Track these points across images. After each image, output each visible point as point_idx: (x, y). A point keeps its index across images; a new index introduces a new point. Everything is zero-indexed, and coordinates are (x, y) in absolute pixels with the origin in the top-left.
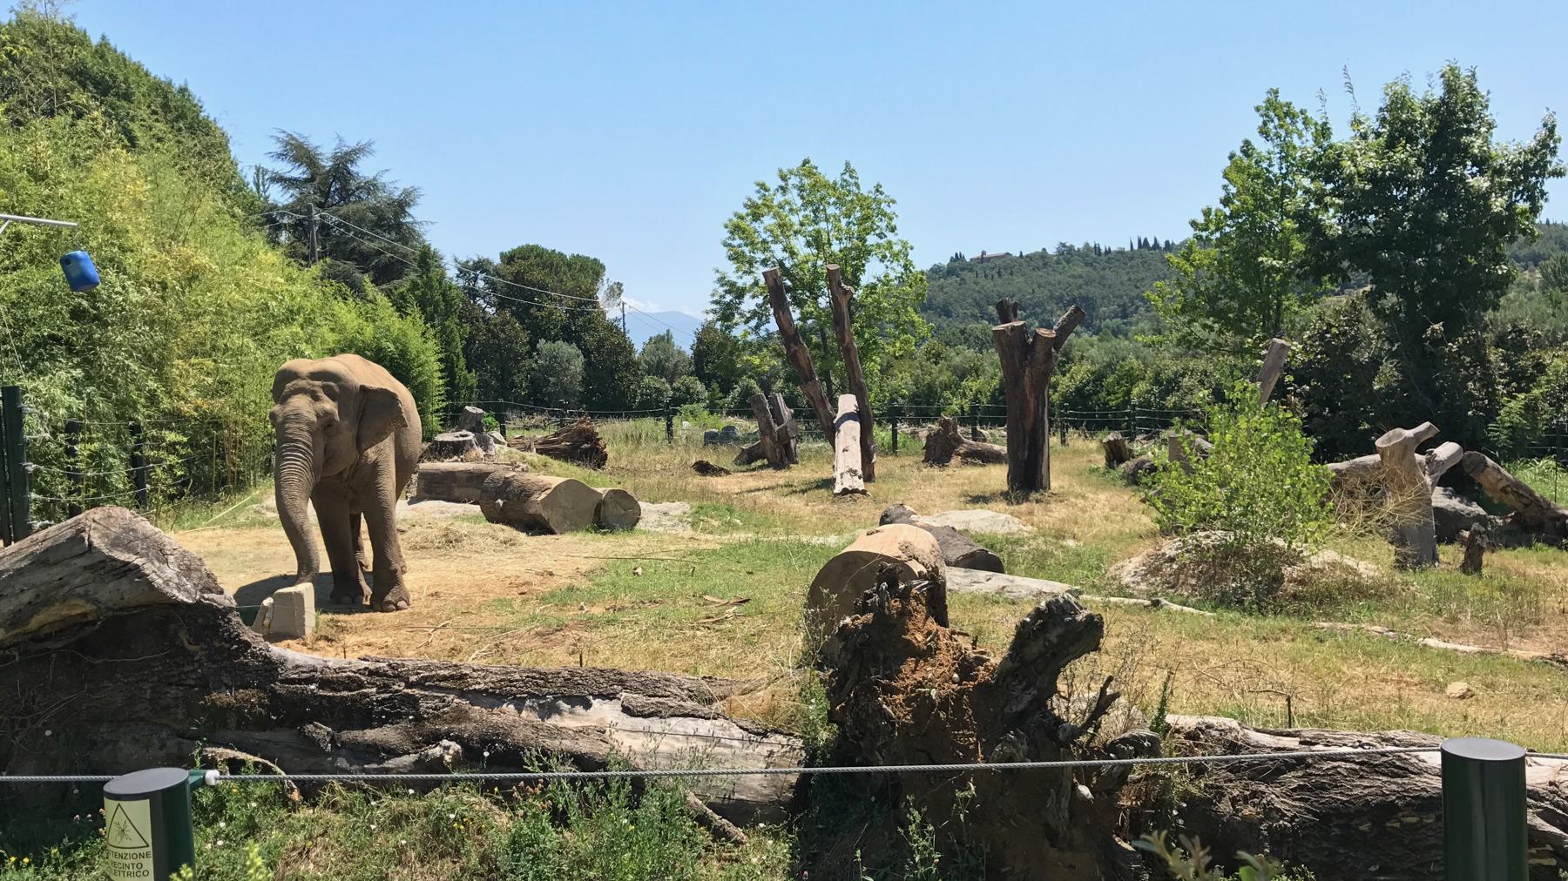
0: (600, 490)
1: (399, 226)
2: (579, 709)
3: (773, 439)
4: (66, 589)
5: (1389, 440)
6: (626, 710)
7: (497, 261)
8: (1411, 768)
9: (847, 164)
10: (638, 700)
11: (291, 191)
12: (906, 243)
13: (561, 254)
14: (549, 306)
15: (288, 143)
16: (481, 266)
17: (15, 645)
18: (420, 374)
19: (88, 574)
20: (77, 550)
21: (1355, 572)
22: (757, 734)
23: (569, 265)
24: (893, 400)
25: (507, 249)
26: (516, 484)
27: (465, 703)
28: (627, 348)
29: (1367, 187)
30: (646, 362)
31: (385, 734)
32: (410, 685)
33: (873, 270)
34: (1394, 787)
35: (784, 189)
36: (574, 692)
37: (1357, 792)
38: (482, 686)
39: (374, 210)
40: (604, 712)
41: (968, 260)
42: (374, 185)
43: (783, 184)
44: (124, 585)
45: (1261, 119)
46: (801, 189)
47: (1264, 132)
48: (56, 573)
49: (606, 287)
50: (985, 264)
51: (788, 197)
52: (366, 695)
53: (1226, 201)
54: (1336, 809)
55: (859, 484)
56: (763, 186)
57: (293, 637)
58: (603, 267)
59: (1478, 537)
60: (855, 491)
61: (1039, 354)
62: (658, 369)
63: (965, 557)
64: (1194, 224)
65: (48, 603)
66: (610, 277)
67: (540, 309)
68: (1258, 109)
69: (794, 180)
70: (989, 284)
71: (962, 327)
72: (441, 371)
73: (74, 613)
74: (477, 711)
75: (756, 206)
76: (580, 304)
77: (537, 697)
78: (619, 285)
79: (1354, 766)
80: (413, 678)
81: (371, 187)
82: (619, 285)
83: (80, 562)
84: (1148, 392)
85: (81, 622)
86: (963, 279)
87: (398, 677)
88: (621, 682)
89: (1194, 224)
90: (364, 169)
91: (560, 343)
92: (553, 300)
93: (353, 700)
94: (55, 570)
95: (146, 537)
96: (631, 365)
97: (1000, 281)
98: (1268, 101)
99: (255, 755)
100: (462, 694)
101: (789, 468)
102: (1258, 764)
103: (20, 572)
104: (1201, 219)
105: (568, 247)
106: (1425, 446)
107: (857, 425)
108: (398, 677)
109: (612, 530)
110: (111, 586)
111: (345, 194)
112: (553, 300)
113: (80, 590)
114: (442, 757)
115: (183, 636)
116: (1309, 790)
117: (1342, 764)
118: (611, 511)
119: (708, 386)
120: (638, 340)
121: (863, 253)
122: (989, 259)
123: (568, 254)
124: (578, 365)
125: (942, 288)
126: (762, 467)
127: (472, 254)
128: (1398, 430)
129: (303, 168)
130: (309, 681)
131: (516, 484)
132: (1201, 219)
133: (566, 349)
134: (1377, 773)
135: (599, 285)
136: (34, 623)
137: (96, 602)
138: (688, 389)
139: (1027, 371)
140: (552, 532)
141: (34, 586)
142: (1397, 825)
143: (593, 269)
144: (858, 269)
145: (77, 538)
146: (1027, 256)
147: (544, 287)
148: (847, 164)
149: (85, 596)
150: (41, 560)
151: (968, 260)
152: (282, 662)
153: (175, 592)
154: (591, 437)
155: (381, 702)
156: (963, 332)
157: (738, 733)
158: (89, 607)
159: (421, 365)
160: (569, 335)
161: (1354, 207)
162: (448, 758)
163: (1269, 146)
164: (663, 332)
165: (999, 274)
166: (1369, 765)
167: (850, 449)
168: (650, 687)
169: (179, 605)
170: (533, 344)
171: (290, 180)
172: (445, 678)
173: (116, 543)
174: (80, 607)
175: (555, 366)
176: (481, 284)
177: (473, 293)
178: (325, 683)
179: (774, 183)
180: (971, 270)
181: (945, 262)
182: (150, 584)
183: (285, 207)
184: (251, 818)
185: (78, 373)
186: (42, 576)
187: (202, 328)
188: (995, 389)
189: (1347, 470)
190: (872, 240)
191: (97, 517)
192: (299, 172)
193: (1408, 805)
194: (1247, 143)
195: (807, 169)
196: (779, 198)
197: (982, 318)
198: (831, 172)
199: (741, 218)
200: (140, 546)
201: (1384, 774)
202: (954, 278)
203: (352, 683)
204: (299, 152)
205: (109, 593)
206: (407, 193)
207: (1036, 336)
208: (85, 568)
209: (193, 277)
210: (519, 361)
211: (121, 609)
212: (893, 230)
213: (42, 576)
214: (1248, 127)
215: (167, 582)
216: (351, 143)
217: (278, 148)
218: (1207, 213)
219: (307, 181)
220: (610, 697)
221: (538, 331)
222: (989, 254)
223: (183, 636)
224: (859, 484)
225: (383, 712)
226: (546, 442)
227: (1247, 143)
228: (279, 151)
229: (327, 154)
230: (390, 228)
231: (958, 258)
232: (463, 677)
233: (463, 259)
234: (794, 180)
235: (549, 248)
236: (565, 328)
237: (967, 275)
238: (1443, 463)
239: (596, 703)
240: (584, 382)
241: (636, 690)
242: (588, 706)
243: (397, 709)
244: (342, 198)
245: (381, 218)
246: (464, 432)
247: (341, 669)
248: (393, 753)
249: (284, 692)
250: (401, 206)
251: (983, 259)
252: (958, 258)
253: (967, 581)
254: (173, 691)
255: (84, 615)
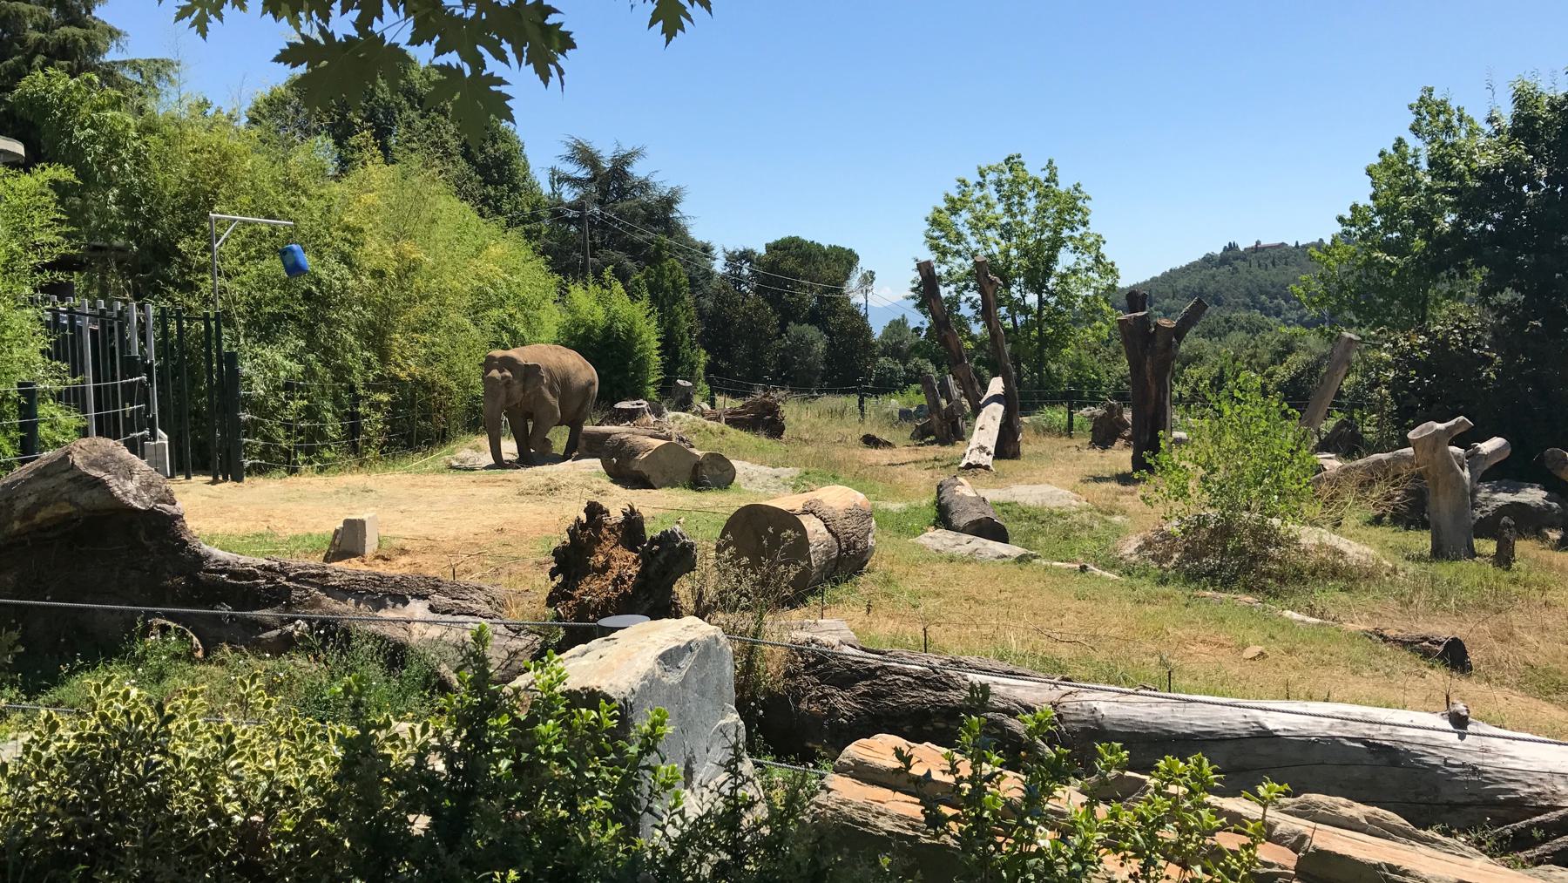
0: (698, 453)
1: (667, 219)
2: (399, 606)
3: (940, 417)
4: (57, 495)
5: (1421, 432)
6: (432, 609)
7: (762, 251)
8: (952, 684)
9: (1050, 162)
10: (438, 599)
11: (576, 190)
12: (1100, 236)
13: (819, 245)
14: (798, 292)
15: (575, 148)
16: (746, 256)
17: (28, 533)
18: (641, 351)
19: (71, 485)
20: (64, 468)
21: (1342, 554)
22: (514, 631)
23: (826, 255)
24: (1118, 385)
25: (771, 241)
26: (628, 445)
27: (322, 595)
28: (865, 330)
29: (1478, 185)
30: (883, 344)
31: (266, 614)
32: (289, 579)
33: (1065, 259)
34: (932, 698)
35: (981, 185)
36: (399, 592)
37: (905, 700)
38: (336, 583)
39: (645, 206)
40: (418, 609)
41: (1242, 249)
42: (647, 185)
43: (981, 180)
44: (95, 493)
45: (1414, 117)
46: (999, 184)
47: (1415, 130)
48: (52, 482)
49: (859, 275)
50: (1259, 254)
51: (986, 191)
52: (258, 584)
53: (1374, 197)
54: (886, 713)
55: (987, 460)
56: (963, 182)
57: (355, 555)
58: (857, 258)
59: (1507, 531)
60: (978, 466)
61: (1160, 344)
62: (894, 351)
63: (972, 523)
64: (1341, 220)
65: (46, 504)
66: (864, 265)
67: (792, 295)
68: (1411, 107)
69: (991, 177)
70: (1261, 273)
71: (1227, 315)
72: (658, 349)
73: (63, 512)
74: (328, 601)
75: (952, 201)
76: (831, 291)
77: (372, 593)
78: (872, 273)
79: (912, 680)
80: (291, 574)
81: (644, 186)
82: (872, 273)
83: (66, 476)
84: (1358, 383)
85: (67, 520)
86: (1235, 269)
87: (282, 572)
88: (436, 587)
89: (1341, 220)
90: (638, 170)
91: (806, 325)
92: (803, 287)
93: (248, 587)
94: (51, 480)
95: (121, 460)
96: (869, 346)
97: (1275, 271)
98: (1421, 99)
99: (178, 623)
100: (323, 588)
101: (953, 444)
102: (1463, 751)
103: (28, 481)
104: (1348, 215)
105: (825, 236)
106: (1465, 440)
107: (1001, 408)
108: (282, 572)
109: (708, 487)
110: (87, 493)
111: (622, 193)
112: (803, 287)
113: (66, 496)
114: (292, 632)
115: (142, 533)
116: (871, 696)
117: (902, 677)
118: (706, 474)
119: (939, 368)
120: (877, 328)
121: (1057, 243)
122: (1264, 248)
123: (825, 244)
124: (820, 347)
125: (1213, 277)
126: (932, 443)
127: (737, 244)
128: (1431, 423)
129: (588, 169)
130: (222, 572)
131: (628, 445)
132: (1348, 215)
133: (811, 332)
134: (927, 687)
135: (853, 272)
136: (39, 517)
137: (76, 505)
138: (920, 370)
139: (1149, 358)
140: (654, 488)
141: (37, 491)
142: (930, 729)
143: (846, 259)
144: (1052, 258)
145: (65, 459)
146: (1304, 246)
147: (797, 276)
148: (1050, 162)
149: (70, 501)
150: (41, 474)
151: (1242, 249)
152: (208, 557)
153: (131, 501)
154: (772, 410)
155: (267, 590)
156: (1227, 321)
157: (501, 629)
158: (72, 509)
159: (643, 343)
160: (815, 318)
161: (1470, 204)
162: (296, 633)
163: (1419, 143)
164: (898, 317)
165: (1274, 264)
166: (922, 681)
167: (987, 428)
168: (457, 591)
169: (136, 510)
170: (783, 326)
171: (575, 179)
172: (313, 576)
173: (93, 464)
174: (67, 509)
175: (801, 346)
176: (746, 272)
177: (738, 281)
178: (234, 574)
179: (973, 178)
180: (1244, 260)
181: (1218, 251)
182: (111, 494)
183: (570, 203)
184: (161, 667)
185: (302, 343)
186: (41, 484)
187: (421, 310)
188: (1215, 378)
189: (1388, 461)
190: (1066, 233)
191: (83, 444)
192: (583, 173)
193: (937, 713)
194: (1400, 141)
195: (1012, 162)
196: (978, 194)
197: (1255, 307)
198: (1035, 169)
199: (940, 212)
200: (112, 467)
201: (930, 688)
202: (1227, 267)
203: (251, 575)
204: (585, 156)
205: (86, 498)
206: (674, 192)
207: (1157, 325)
208: (69, 480)
209: (413, 268)
210: (770, 342)
211: (94, 511)
212: (1085, 224)
213: (41, 484)
214: (1401, 122)
215: (125, 494)
216: (627, 148)
217: (567, 151)
218: (1354, 208)
219: (590, 180)
220: (425, 597)
221: (789, 313)
222: (1264, 243)
223: (142, 533)
224: (987, 460)
225: (266, 598)
226: (734, 413)
227: (1400, 141)
228: (568, 154)
229: (606, 154)
230: (657, 223)
231: (1232, 247)
232: (327, 575)
233: (730, 250)
234: (991, 177)
235: (809, 239)
236: (813, 312)
237: (1239, 264)
238: (1486, 457)
239: (413, 602)
240: (827, 361)
241: (445, 594)
242: (406, 603)
243: (278, 596)
244: (619, 196)
245: (652, 213)
246: (641, 401)
247: (246, 565)
248: (268, 628)
249: (203, 578)
250: (669, 202)
251: (1257, 249)
252: (1232, 247)
253: (953, 543)
254: (133, 574)
255: (70, 514)
